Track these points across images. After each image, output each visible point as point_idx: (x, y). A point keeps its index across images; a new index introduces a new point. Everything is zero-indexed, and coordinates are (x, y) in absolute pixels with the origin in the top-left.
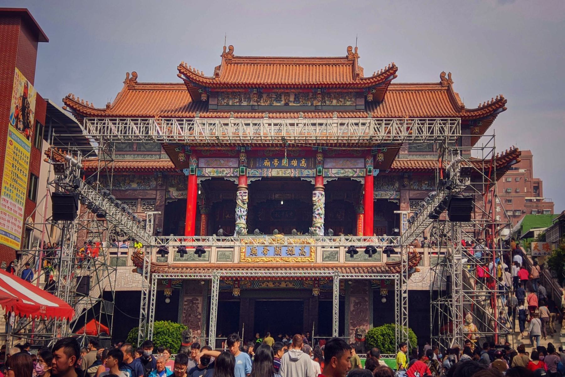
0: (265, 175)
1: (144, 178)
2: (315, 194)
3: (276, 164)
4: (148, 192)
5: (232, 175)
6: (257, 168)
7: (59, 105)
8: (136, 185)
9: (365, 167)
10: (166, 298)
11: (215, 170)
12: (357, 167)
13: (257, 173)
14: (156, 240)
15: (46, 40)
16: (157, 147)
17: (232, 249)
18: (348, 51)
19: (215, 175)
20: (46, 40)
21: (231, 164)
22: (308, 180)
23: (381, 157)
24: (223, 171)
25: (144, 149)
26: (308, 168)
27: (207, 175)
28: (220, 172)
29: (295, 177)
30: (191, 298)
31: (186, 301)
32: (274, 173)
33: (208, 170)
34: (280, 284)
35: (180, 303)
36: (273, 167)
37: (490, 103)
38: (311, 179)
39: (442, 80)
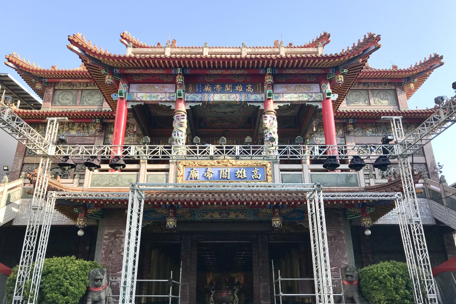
0: (206, 99)
1: (84, 126)
2: (266, 117)
4: (87, 138)
5: (168, 100)
6: (198, 93)
10: (79, 229)
11: (149, 94)
12: (312, 92)
13: (197, 98)
14: (57, 149)
16: (99, 103)
17: (167, 173)
19: (148, 99)
21: (166, 90)
22: (256, 105)
25: (87, 104)
27: (138, 100)
28: (154, 97)
29: (241, 102)
31: (107, 235)
32: (217, 97)
33: (139, 95)
34: (229, 214)
35: (99, 237)
37: (423, 62)
38: (260, 104)
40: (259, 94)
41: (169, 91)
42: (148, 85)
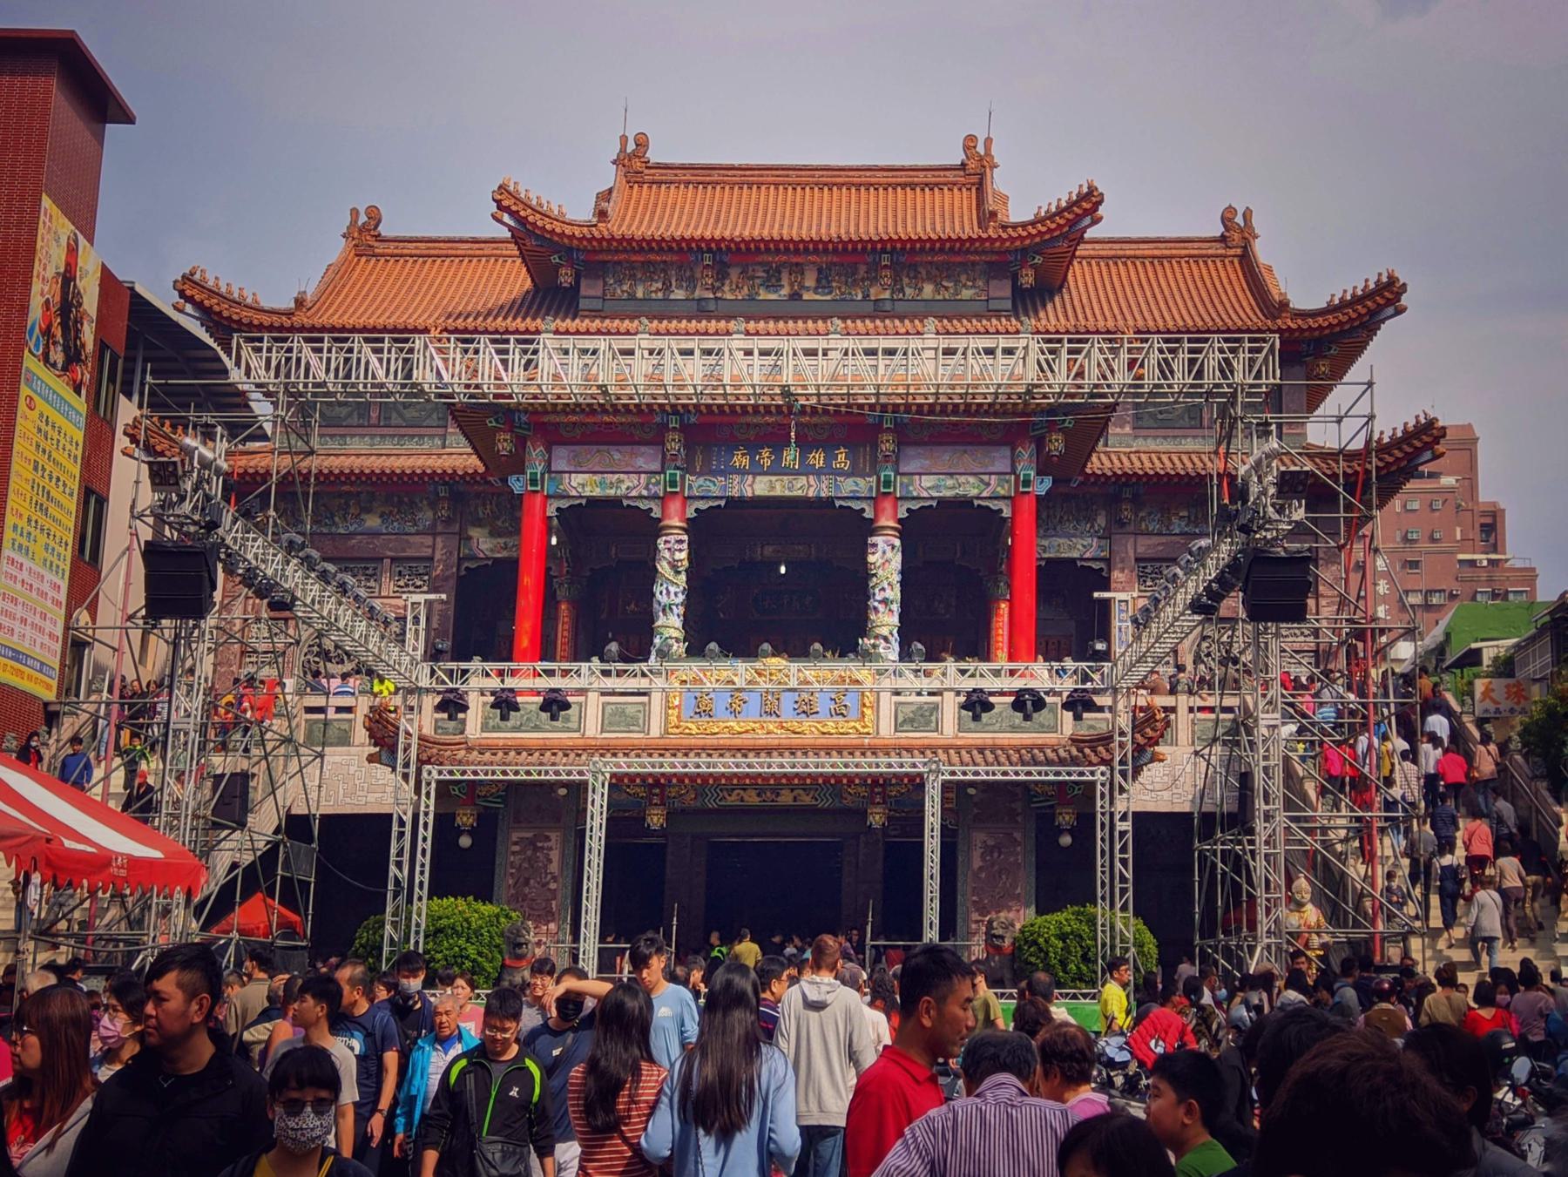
1: (401, 502)
2: (875, 545)
3: (767, 463)
4: (411, 539)
5: (645, 493)
6: (714, 473)
7: (164, 299)
8: (379, 521)
9: (1013, 472)
11: (597, 478)
12: (991, 469)
14: (433, 672)
15: (127, 118)
17: (645, 699)
18: (966, 148)
19: (597, 492)
20: (127, 118)
21: (640, 463)
22: (856, 505)
23: (1056, 444)
24: (620, 481)
25: (400, 421)
26: (853, 472)
27: (574, 493)
28: (611, 485)
29: (819, 499)
30: (530, 835)
31: (516, 843)
32: (761, 487)
33: (577, 479)
34: (778, 795)
35: (500, 848)
36: (756, 470)
37: (1360, 293)
38: (864, 505)
39: (1227, 228)
40: (863, 476)
41: (646, 467)
42: (595, 448)
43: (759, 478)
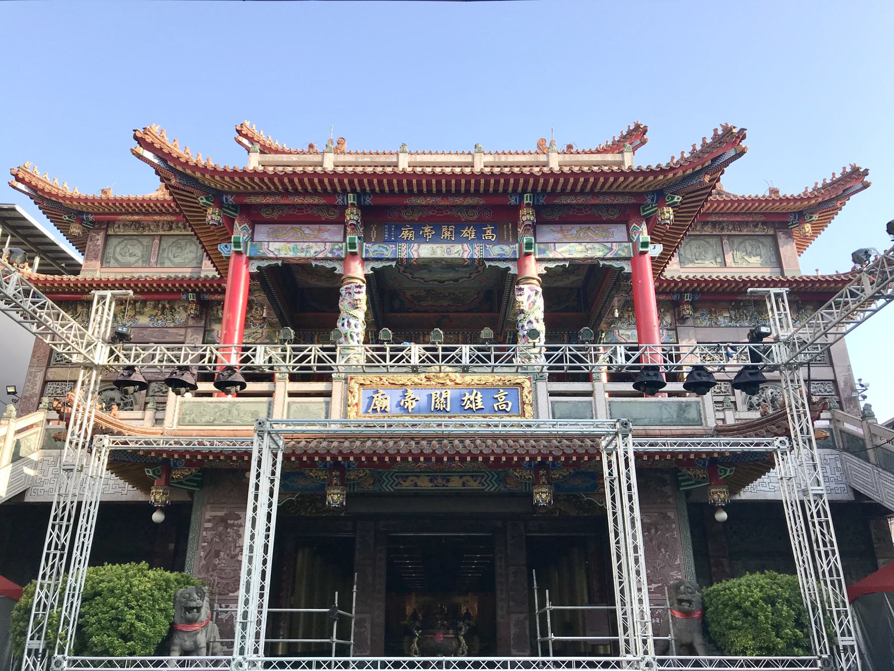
1: (164, 308)
4: (170, 330)
5: (330, 255)
8: (148, 319)
11: (291, 245)
12: (611, 239)
13: (385, 252)
14: (112, 352)
17: (327, 399)
19: (290, 255)
21: (326, 236)
22: (503, 265)
24: (309, 247)
25: (171, 265)
27: (271, 255)
29: (472, 260)
30: (221, 514)
31: (209, 521)
32: (425, 251)
33: (273, 246)
34: (448, 481)
35: (194, 525)
37: (828, 181)
41: (331, 239)
42: (289, 226)
43: (422, 246)
